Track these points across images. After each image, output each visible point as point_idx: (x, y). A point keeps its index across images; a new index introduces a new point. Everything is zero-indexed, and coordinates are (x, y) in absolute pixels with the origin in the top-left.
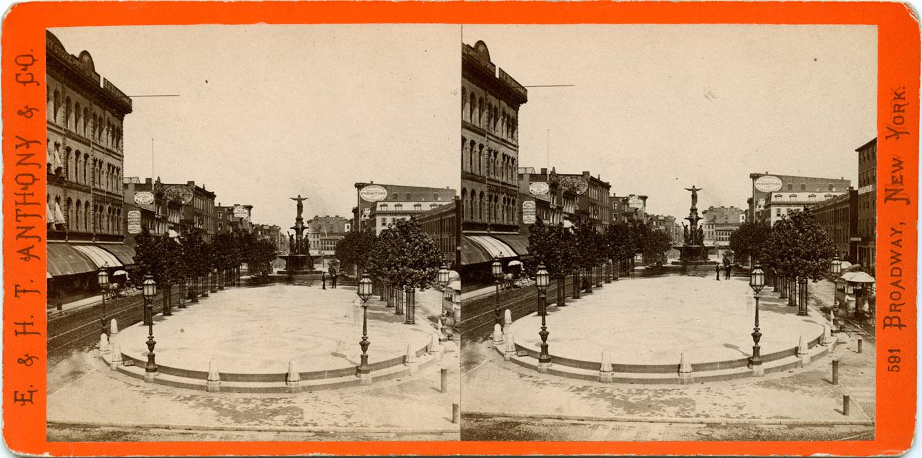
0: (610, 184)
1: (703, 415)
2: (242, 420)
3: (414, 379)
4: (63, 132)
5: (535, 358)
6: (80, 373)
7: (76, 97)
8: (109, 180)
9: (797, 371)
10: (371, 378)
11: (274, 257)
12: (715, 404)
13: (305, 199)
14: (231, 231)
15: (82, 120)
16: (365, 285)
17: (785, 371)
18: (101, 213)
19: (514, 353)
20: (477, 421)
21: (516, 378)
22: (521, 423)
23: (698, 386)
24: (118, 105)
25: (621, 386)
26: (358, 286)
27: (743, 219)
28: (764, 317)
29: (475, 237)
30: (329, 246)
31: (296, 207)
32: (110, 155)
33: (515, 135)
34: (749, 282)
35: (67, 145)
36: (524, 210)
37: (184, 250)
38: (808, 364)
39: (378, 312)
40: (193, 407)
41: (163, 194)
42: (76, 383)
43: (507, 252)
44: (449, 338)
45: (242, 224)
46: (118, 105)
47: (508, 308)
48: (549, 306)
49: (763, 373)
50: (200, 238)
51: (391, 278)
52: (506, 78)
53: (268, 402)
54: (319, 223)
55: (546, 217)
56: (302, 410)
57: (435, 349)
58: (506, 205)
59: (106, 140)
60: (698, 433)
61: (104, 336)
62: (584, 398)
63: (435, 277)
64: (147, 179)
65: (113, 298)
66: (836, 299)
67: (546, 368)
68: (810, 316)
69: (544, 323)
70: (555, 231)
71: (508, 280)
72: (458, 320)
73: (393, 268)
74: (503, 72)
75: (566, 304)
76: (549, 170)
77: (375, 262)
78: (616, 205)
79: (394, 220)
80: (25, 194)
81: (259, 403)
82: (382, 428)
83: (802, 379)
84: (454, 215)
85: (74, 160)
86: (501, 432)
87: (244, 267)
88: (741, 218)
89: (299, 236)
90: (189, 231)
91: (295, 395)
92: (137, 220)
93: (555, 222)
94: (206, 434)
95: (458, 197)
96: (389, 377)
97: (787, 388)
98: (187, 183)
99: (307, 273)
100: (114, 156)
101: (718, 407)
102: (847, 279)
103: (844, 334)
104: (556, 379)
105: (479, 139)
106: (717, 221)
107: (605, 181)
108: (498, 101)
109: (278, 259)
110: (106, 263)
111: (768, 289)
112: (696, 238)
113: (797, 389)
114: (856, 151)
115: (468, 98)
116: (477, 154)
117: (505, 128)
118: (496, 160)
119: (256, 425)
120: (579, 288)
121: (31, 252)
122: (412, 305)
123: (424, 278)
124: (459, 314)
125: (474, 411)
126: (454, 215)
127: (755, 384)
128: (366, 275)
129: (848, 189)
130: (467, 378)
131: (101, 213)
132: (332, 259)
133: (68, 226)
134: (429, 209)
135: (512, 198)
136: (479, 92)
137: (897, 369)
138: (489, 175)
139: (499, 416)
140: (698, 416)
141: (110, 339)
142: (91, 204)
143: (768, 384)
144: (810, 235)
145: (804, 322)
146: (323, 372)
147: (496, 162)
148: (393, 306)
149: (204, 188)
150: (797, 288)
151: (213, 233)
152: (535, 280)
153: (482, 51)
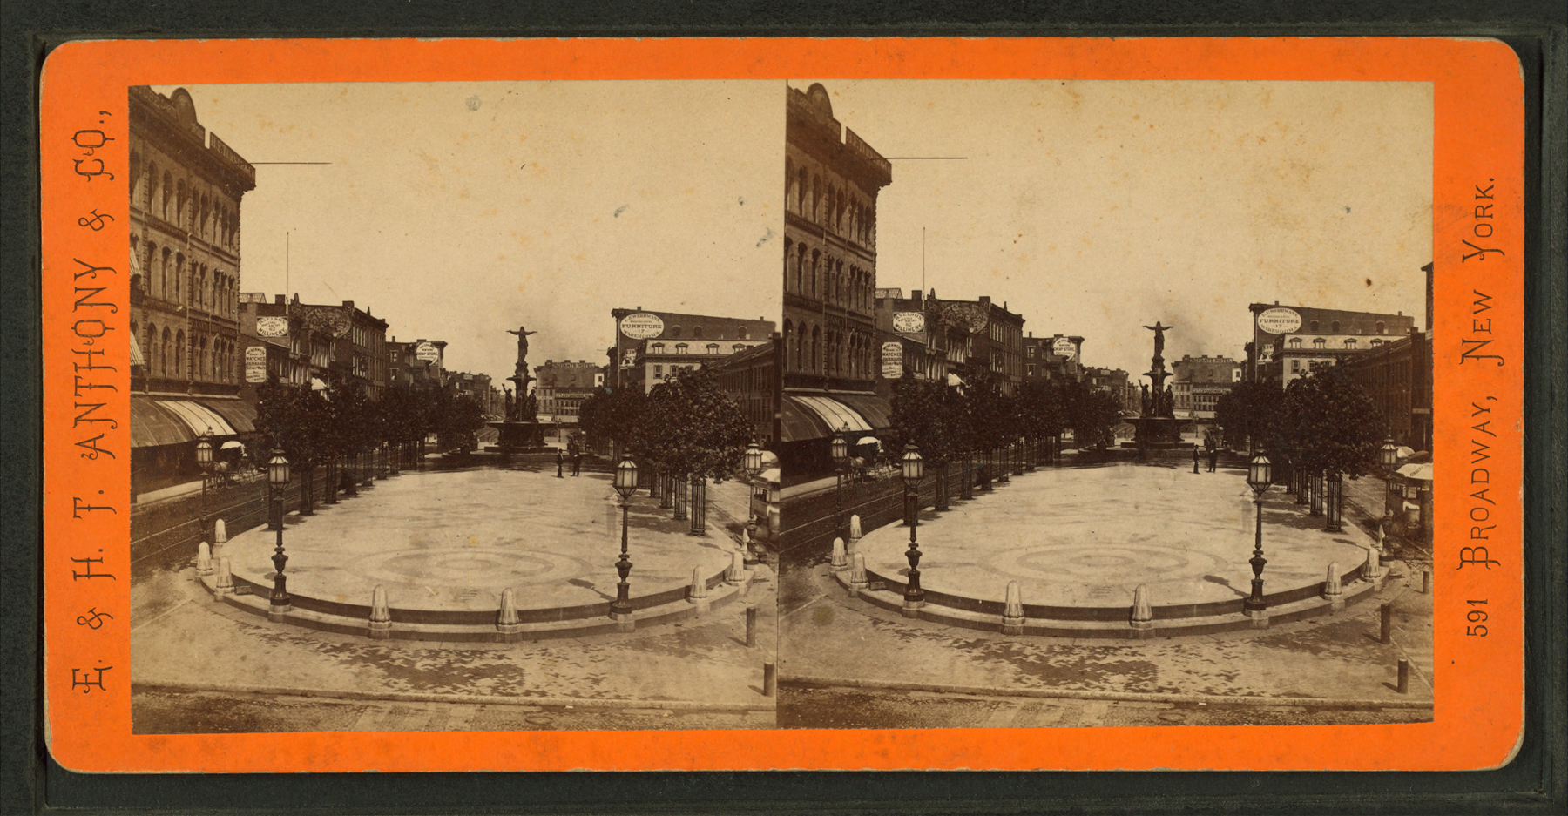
0: (387, 322)
1: (537, 693)
2: (1058, 681)
3: (703, 624)
4: (142, 218)
6: (165, 604)
7: (164, 162)
8: (217, 295)
9: (1324, 621)
10: (632, 622)
11: (479, 425)
12: (1189, 672)
13: (1167, 328)
14: (412, 382)
16: (626, 473)
20: (803, 692)
21: (867, 625)
22: (874, 697)
23: (527, 647)
24: (238, 178)
25: (1036, 640)
26: (615, 472)
27: (1238, 376)
29: (805, 399)
30: (570, 408)
32: (219, 257)
33: (871, 235)
34: (1246, 477)
35: (150, 239)
36: (247, 361)
39: (644, 515)
40: (346, 662)
43: (220, 428)
44: (761, 559)
45: (1066, 367)
46: (238, 178)
47: (221, 516)
50: (362, 392)
51: (668, 462)
54: (553, 372)
55: (920, 367)
56: (521, 669)
57: (738, 577)
58: (219, 351)
59: (213, 232)
61: (204, 546)
62: (977, 658)
63: (739, 461)
66: (753, 511)
67: (281, 613)
68: (710, 537)
69: (280, 542)
70: (296, 396)
71: (220, 472)
73: (1306, 441)
74: (853, 133)
75: (950, 507)
76: (290, 297)
77: (642, 435)
78: (395, 355)
79: (674, 369)
80: (89, 353)
81: (452, 657)
83: (1333, 635)
84: (771, 363)
85: (160, 265)
87: (1068, 436)
88: (1234, 375)
89: (1157, 387)
91: (510, 646)
92: (260, 361)
95: (779, 334)
96: (663, 619)
97: (1305, 648)
98: (341, 304)
99: (533, 451)
101: (1194, 677)
102: (1407, 475)
103: (1400, 563)
104: (931, 628)
105: (812, 242)
107: (1015, 313)
108: (208, 184)
109: (486, 427)
110: (210, 428)
112: (524, 410)
113: (1323, 650)
114: (1423, 269)
115: (795, 175)
116: (810, 265)
117: (855, 225)
118: (205, 280)
119: (448, 692)
120: (970, 483)
121: (100, 444)
122: (701, 505)
123: (722, 463)
124: (777, 521)
125: (166, 681)
126: (771, 363)
128: (628, 456)
129: (770, 335)
130: (786, 623)
132: (573, 430)
133: (149, 369)
134: (732, 352)
136: (815, 167)
137: (1484, 631)
139: (204, 690)
142: (187, 334)
143: (1275, 642)
145: (1335, 543)
146: (556, 609)
147: (204, 285)
149: (369, 312)
150: (1325, 488)
151: (382, 384)
152: (901, 468)
153: (819, 100)
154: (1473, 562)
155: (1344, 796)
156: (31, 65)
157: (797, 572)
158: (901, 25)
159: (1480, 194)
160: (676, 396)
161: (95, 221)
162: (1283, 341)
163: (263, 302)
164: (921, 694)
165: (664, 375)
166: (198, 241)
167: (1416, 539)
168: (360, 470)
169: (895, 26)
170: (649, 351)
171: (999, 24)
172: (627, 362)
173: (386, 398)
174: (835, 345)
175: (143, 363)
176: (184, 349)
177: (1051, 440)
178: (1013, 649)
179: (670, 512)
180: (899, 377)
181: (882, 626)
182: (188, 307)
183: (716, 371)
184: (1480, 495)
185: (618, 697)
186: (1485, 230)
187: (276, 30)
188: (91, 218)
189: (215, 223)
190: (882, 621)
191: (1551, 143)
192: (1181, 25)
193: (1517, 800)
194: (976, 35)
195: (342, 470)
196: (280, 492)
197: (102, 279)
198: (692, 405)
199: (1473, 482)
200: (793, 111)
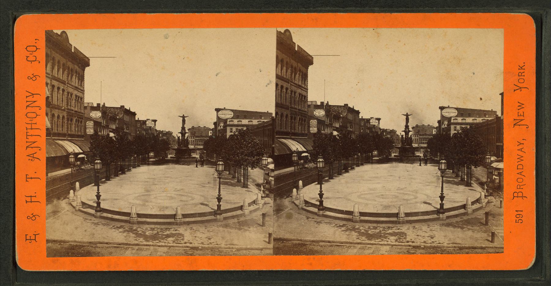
0: (136, 113)
2: (372, 239)
4: (50, 76)
5: (316, 208)
6: (58, 212)
7: (58, 57)
8: (76, 103)
9: (465, 218)
10: (222, 218)
11: (168, 149)
13: (186, 117)
14: (145, 134)
15: (61, 70)
16: (443, 164)
17: (458, 218)
18: (305, 122)
19: (304, 205)
20: (282, 243)
24: (84, 62)
25: (364, 224)
26: (216, 166)
27: (435, 132)
28: (446, 187)
29: (283, 140)
31: (182, 121)
32: (77, 90)
33: (306, 82)
35: (53, 84)
36: (87, 127)
37: (118, 144)
38: (248, 215)
39: (226, 181)
40: (122, 232)
41: (106, 113)
42: (55, 218)
43: (77, 150)
44: (267, 196)
45: (375, 129)
46: (84, 62)
47: (77, 181)
48: (324, 179)
49: (222, 220)
52: (301, 51)
53: (164, 230)
55: (323, 129)
56: (183, 235)
58: (77, 123)
59: (75, 81)
60: (408, 252)
61: (72, 191)
62: (343, 231)
63: (260, 162)
64: (97, 104)
65: (77, 170)
66: (264, 179)
67: (99, 215)
68: (473, 187)
69: (98, 190)
71: (77, 165)
72: (272, 186)
74: (77, 49)
76: (102, 104)
77: (226, 152)
78: (363, 123)
80: (31, 124)
81: (159, 230)
82: (452, 245)
83: (468, 222)
84: (271, 127)
85: (56, 93)
86: (296, 249)
87: (375, 153)
89: (406, 136)
90: (121, 133)
92: (91, 127)
93: (328, 132)
94: (351, 246)
95: (274, 117)
96: (233, 217)
97: (459, 227)
99: (187, 158)
100: (303, 89)
102: (495, 166)
104: (103, 221)
105: (285, 85)
106: (420, 133)
107: (357, 110)
108: (73, 65)
109: (171, 150)
110: (74, 150)
111: (448, 171)
112: (184, 144)
113: (465, 228)
114: (500, 94)
115: (279, 61)
116: (285, 93)
117: (300, 79)
118: (72, 98)
119: (380, 241)
121: (35, 156)
122: (246, 177)
123: (254, 162)
124: (273, 182)
126: (271, 127)
127: (441, 225)
128: (221, 160)
129: (271, 118)
130: (276, 219)
131: (305, 122)
132: (201, 151)
133: (52, 129)
134: (257, 123)
135: (80, 120)
138: (291, 105)
139: (72, 242)
140: (185, 243)
141: (298, 192)
142: (66, 117)
143: (448, 225)
144: (250, 143)
145: (469, 190)
147: (295, 98)
148: (459, 176)
149: (130, 109)
150: (466, 171)
151: (134, 134)
152: (94, 165)
153: (288, 35)
154: (517, 197)
155: (472, 279)
156: (11, 23)
157: (280, 201)
158: (317, 9)
159: (520, 68)
160: (238, 139)
161: (34, 77)
162: (451, 119)
163: (92, 106)
164: (323, 243)
165: (233, 132)
166: (293, 83)
167: (497, 189)
168: (126, 165)
169: (315, 9)
170: (228, 123)
171: (351, 8)
172: (220, 127)
173: (136, 140)
174: (294, 121)
175: (50, 127)
176: (65, 122)
177: (369, 154)
178: (356, 227)
179: (236, 180)
180: (316, 132)
181: (310, 219)
182: (66, 108)
183: (252, 130)
184: (520, 173)
185: (217, 244)
186: (522, 81)
187: (97, 10)
188: (32, 76)
189: (76, 78)
190: (310, 218)
191: (545, 50)
192: (415, 9)
193: (533, 280)
194: (343, 12)
195: (120, 165)
196: (98, 173)
197: (36, 98)
198: (243, 142)
199: (518, 169)
200: (279, 39)
